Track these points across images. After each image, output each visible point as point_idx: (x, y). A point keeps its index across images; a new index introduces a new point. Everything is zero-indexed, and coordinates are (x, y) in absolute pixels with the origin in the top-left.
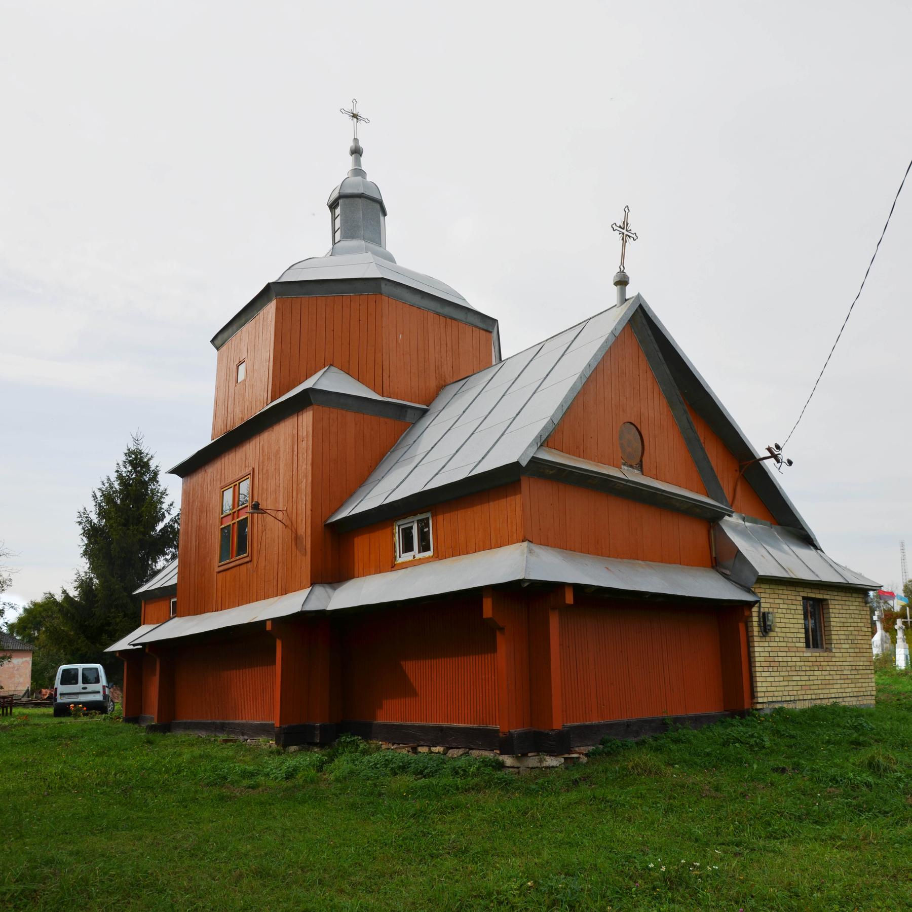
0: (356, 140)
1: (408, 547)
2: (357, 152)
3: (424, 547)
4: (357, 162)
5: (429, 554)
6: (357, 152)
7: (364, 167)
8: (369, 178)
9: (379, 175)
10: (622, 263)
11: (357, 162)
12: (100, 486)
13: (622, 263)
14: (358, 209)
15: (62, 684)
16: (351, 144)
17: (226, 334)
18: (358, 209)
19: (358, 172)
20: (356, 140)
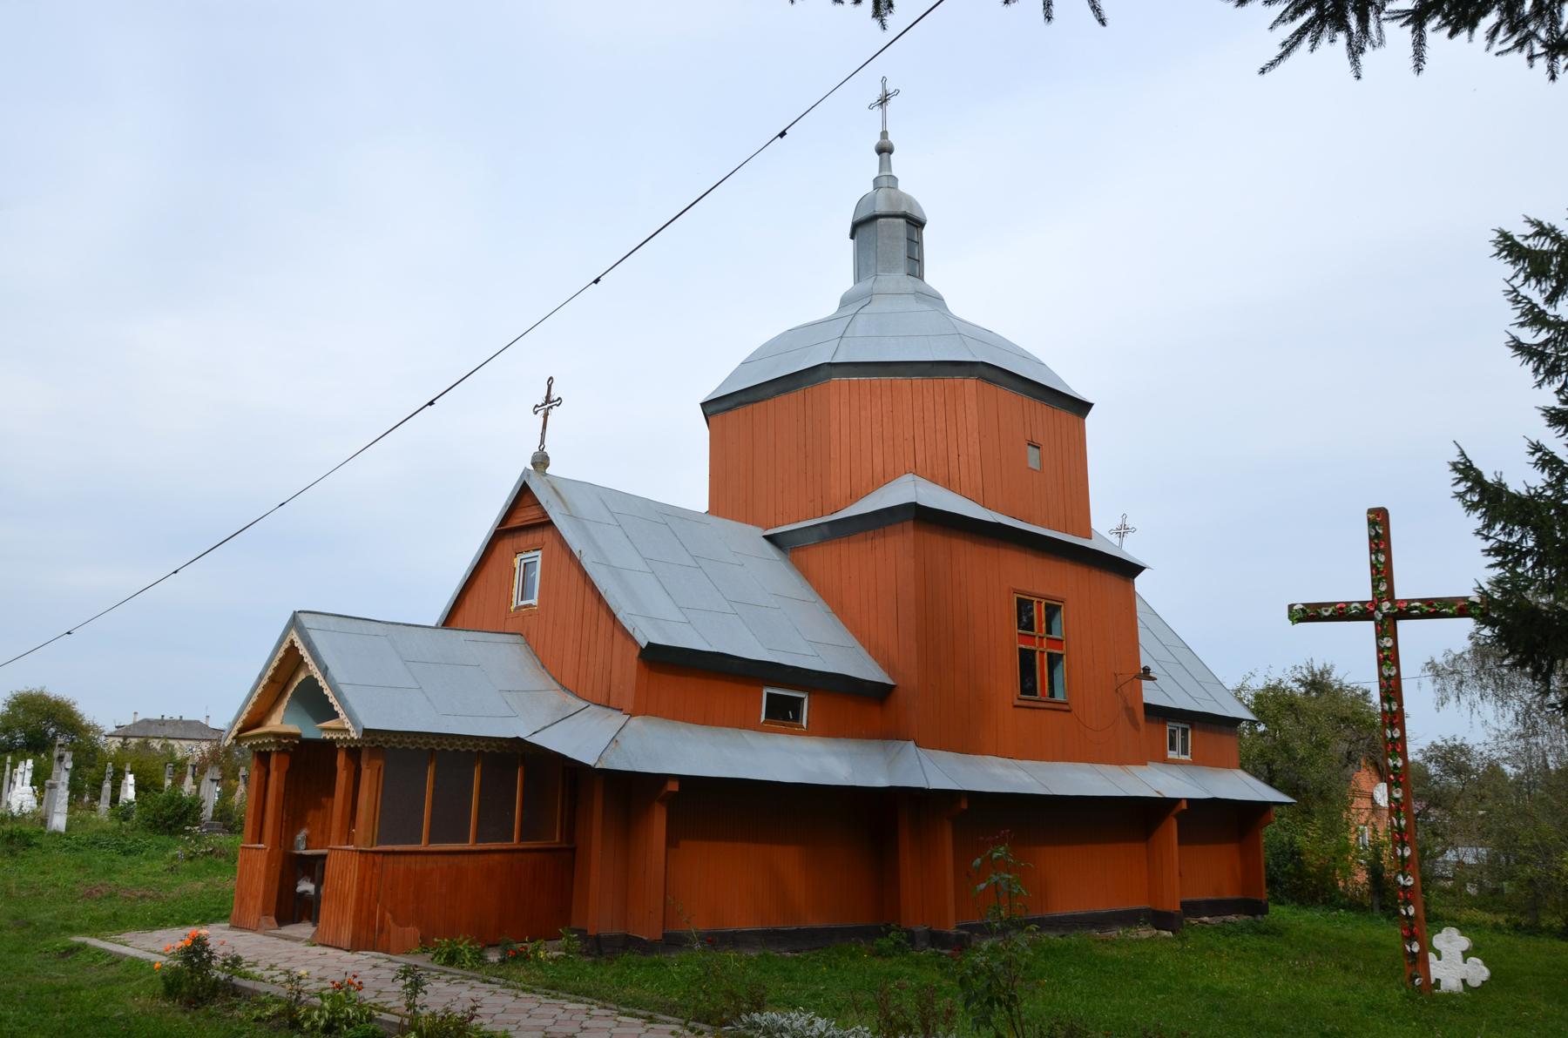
0: (884, 134)
1: (1173, 747)
2: (884, 150)
3: (1185, 752)
4: (885, 165)
5: (1188, 758)
6: (884, 150)
7: (895, 171)
8: (902, 187)
9: (916, 181)
10: (542, 442)
11: (885, 165)
12: (1518, 312)
13: (542, 442)
14: (889, 232)
15: (769, 695)
16: (877, 139)
17: (743, 398)
18: (889, 232)
19: (885, 181)
20: (884, 134)
